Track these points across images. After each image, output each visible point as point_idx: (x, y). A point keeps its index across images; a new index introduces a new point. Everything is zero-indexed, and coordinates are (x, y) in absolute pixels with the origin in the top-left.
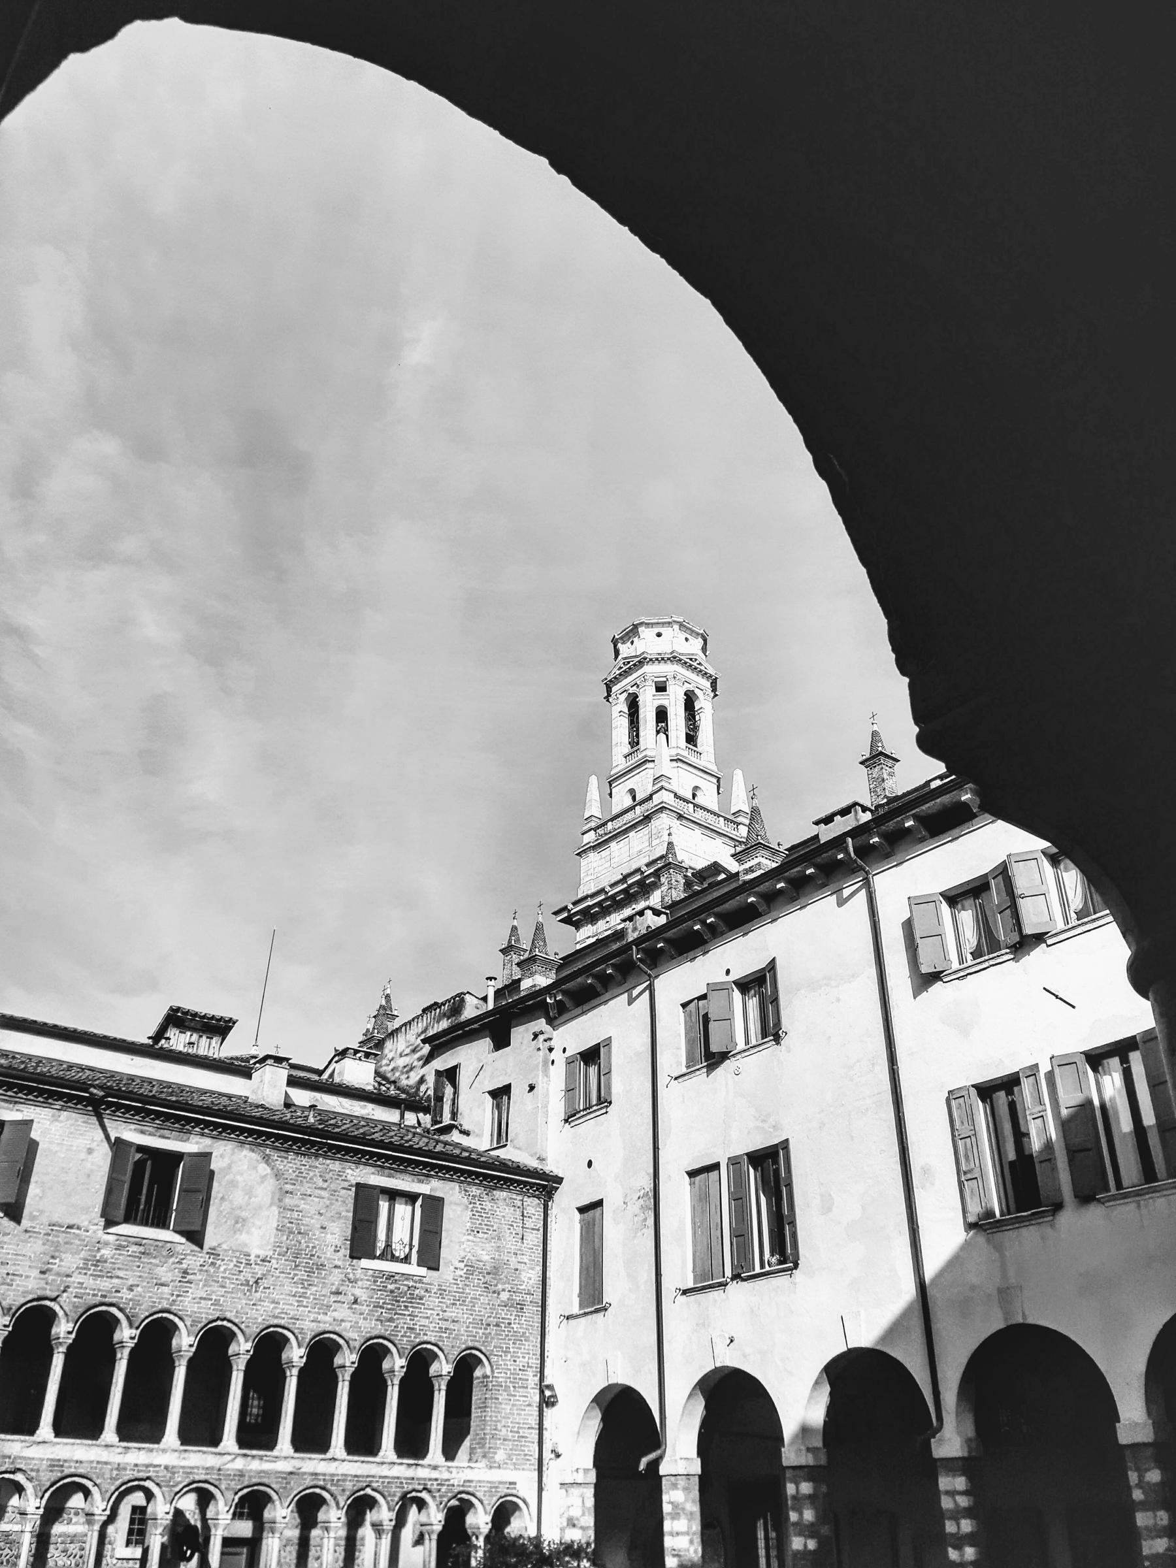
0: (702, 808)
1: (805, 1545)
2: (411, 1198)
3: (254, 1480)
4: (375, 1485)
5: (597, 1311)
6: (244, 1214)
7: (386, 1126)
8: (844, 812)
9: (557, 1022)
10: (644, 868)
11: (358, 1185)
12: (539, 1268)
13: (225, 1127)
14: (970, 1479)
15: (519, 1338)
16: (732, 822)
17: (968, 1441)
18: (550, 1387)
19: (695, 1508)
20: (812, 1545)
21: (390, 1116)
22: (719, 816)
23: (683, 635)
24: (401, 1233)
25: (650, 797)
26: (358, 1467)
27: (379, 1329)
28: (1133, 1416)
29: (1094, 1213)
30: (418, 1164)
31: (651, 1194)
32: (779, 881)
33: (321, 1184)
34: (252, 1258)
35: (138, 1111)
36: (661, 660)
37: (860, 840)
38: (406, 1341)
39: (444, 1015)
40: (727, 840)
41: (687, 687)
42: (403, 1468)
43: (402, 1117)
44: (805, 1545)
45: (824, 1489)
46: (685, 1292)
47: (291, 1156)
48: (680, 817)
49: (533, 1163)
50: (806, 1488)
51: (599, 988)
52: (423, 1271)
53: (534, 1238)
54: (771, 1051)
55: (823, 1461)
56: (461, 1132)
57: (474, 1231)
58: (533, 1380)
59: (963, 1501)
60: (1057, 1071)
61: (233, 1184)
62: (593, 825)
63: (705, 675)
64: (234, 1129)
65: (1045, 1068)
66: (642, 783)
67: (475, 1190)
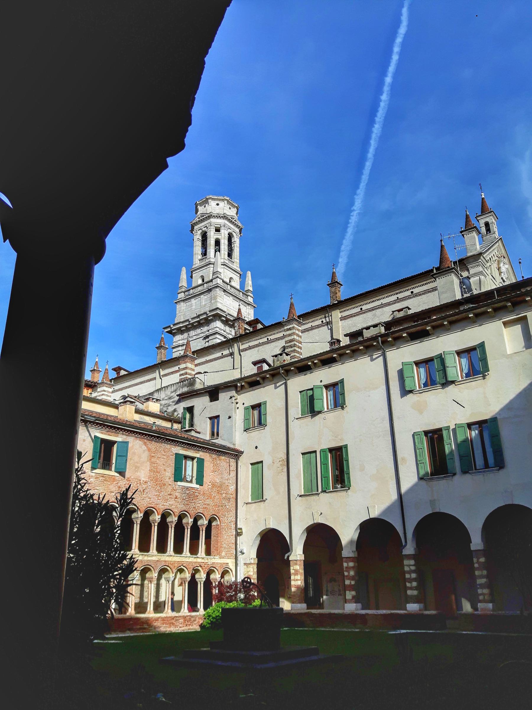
0: (233, 287)
1: (351, 583)
2: (193, 459)
3: (146, 564)
4: (184, 565)
5: (261, 501)
6: (138, 465)
7: (167, 428)
8: (375, 326)
9: (239, 393)
10: (208, 313)
11: (176, 454)
12: (235, 485)
13: (131, 431)
14: (415, 561)
15: (229, 511)
16: (245, 294)
17: (415, 549)
18: (241, 529)
19: (302, 571)
20: (353, 583)
21: (168, 425)
22: (240, 291)
23: (229, 206)
24: (189, 472)
25: (211, 281)
26: (177, 558)
27: (184, 508)
28: (477, 542)
29: (468, 477)
30: (195, 446)
31: (285, 460)
32: (348, 350)
33: (163, 453)
34: (142, 481)
35: (101, 425)
36: (218, 217)
37: (384, 339)
38: (193, 513)
39: (186, 385)
40: (243, 302)
41: (229, 230)
42: (193, 559)
43: (172, 425)
44: (351, 583)
45: (357, 564)
46: (301, 496)
47: (153, 443)
48: (225, 291)
49: (232, 446)
50: (351, 564)
51: (261, 381)
52: (198, 486)
53: (233, 474)
54: (339, 412)
55: (356, 556)
56: (196, 432)
57: (214, 471)
58: (233, 527)
59: (413, 568)
60: (457, 429)
61: (134, 453)
62: (183, 290)
63: (237, 226)
64: (134, 432)
65: (452, 427)
66: (208, 273)
67: (214, 456)
